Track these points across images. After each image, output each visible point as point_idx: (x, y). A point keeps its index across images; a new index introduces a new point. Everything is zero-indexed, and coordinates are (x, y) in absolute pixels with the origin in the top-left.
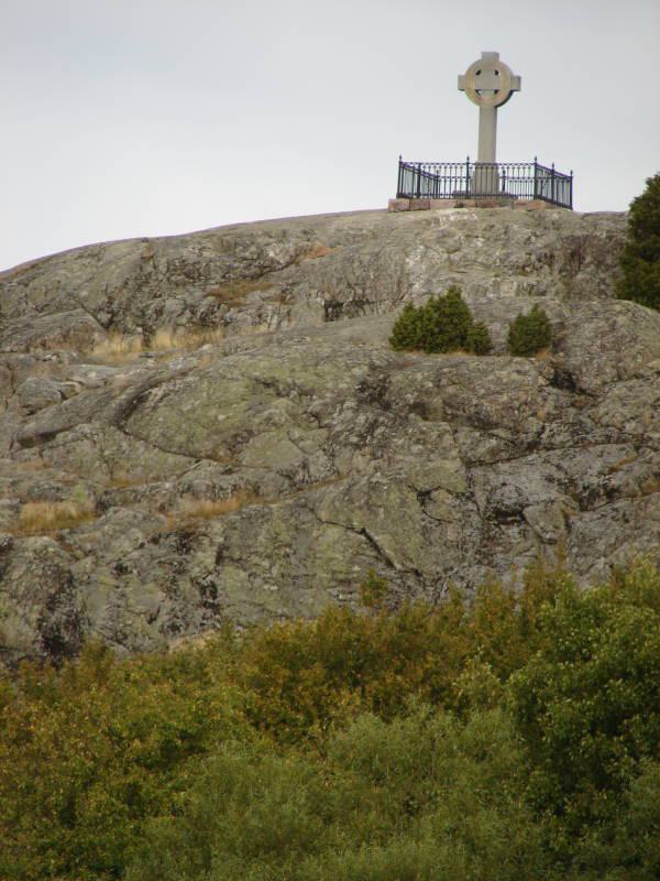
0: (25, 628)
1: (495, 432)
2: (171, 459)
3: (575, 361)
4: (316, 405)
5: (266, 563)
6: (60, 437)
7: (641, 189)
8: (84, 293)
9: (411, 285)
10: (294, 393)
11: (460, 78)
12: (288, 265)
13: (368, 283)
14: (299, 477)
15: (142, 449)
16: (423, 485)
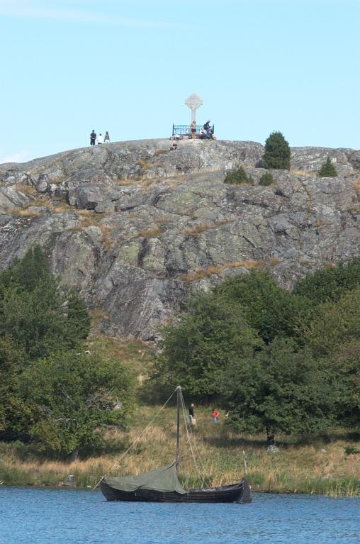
0: (160, 265)
2: (174, 215)
3: (282, 187)
4: (215, 200)
6: (135, 209)
7: (286, 139)
9: (203, 163)
11: (186, 101)
16: (256, 224)
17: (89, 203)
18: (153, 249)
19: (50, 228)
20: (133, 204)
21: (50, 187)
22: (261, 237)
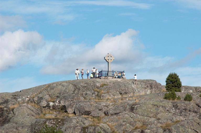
1: (198, 113)
12: (100, 87)
13: (126, 90)
14: (173, 120)
15: (138, 116)
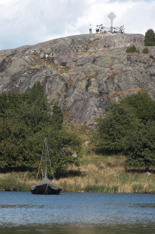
0: (96, 91)
2: (102, 68)
4: (121, 61)
5: (124, 82)
8: (65, 45)
10: (117, 59)
16: (141, 71)
17: (63, 63)
18: (92, 83)
19: (45, 74)
20: (83, 63)
21: (45, 56)
22: (143, 77)
